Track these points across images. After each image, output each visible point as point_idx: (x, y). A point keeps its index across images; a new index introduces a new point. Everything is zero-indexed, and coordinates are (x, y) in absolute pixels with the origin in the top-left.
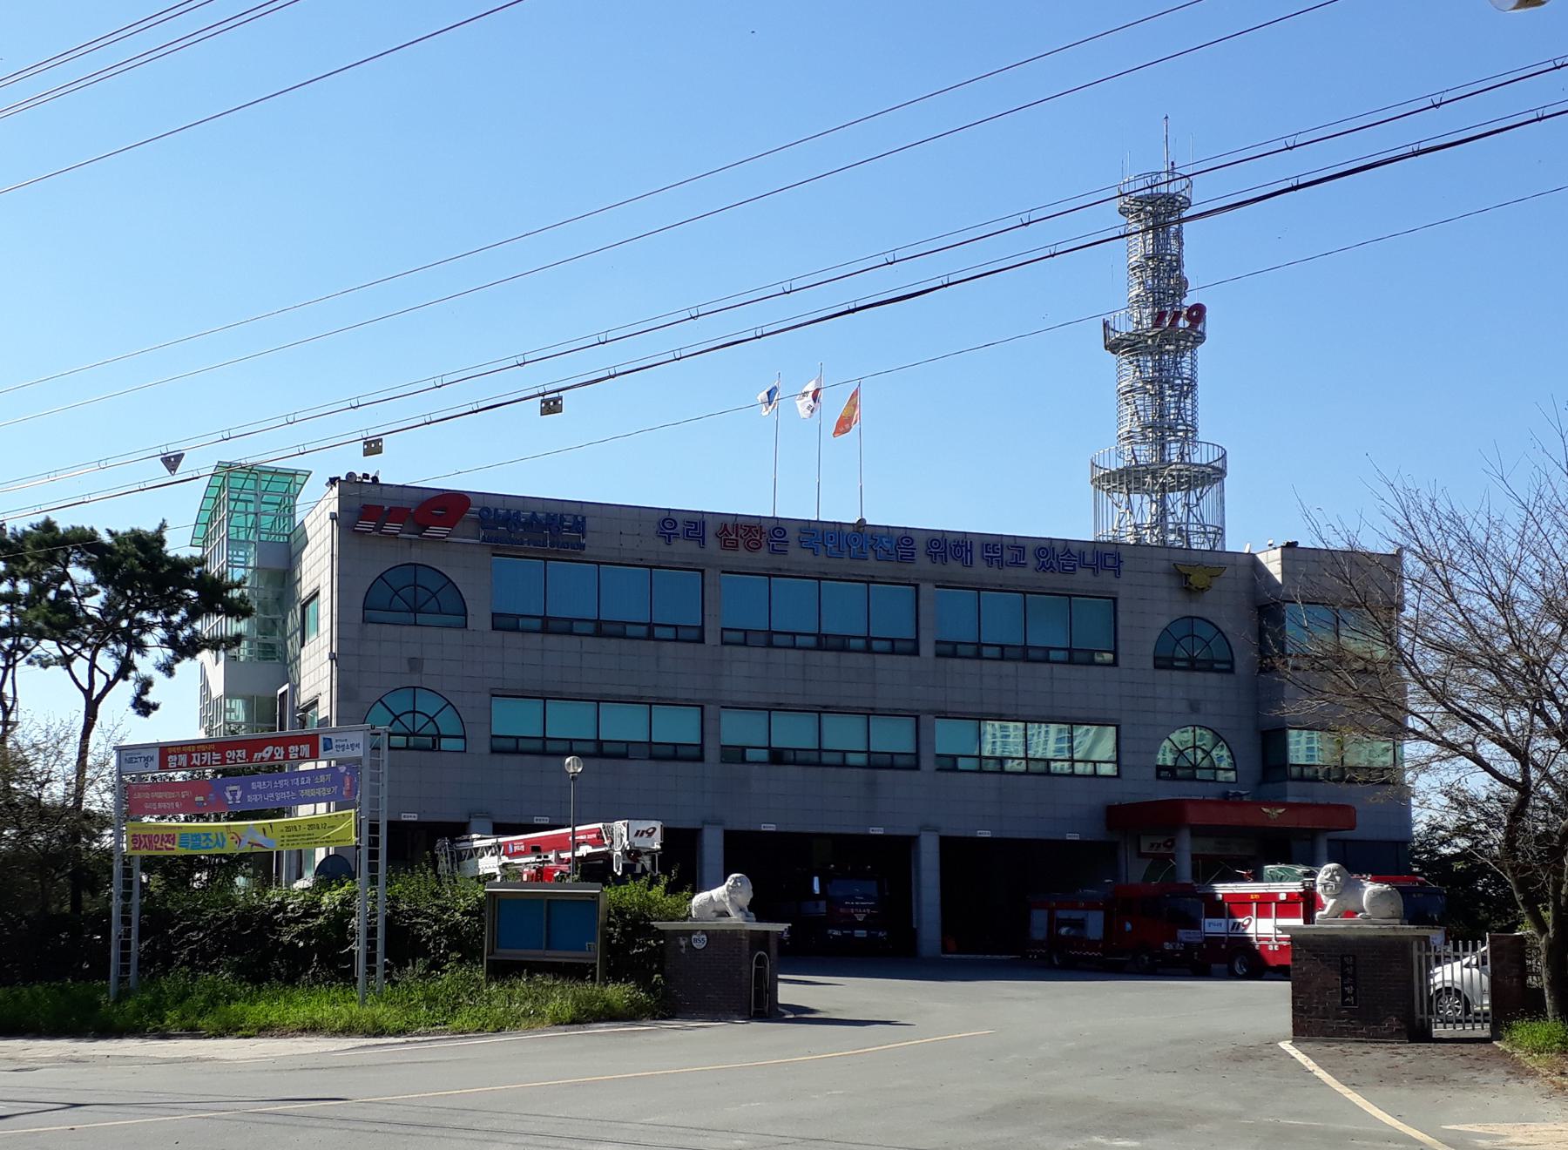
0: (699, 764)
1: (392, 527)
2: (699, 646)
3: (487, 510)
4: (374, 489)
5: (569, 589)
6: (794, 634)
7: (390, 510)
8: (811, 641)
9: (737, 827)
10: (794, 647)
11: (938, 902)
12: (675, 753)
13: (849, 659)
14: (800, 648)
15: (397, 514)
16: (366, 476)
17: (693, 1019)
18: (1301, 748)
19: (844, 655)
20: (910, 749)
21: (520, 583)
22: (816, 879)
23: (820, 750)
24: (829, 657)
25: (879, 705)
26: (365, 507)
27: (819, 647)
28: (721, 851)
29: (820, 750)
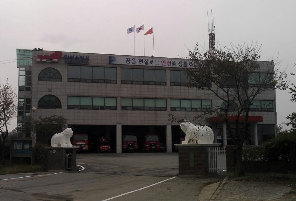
0: (116, 111)
1: (45, 60)
2: (116, 84)
3: (66, 55)
4: (41, 52)
5: (86, 72)
6: (138, 81)
7: (44, 56)
8: (142, 83)
9: (125, 124)
10: (138, 84)
11: (98, 124)
12: (110, 108)
13: (150, 87)
14: (139, 84)
15: (46, 57)
16: (39, 49)
17: (136, 126)
18: (225, 113)
19: (149, 86)
20: (165, 106)
21: (75, 71)
22: (174, 144)
23: (144, 107)
24: (146, 86)
25: (158, 96)
26: (38, 55)
27: (144, 84)
28: (100, 124)
29: (144, 107)
